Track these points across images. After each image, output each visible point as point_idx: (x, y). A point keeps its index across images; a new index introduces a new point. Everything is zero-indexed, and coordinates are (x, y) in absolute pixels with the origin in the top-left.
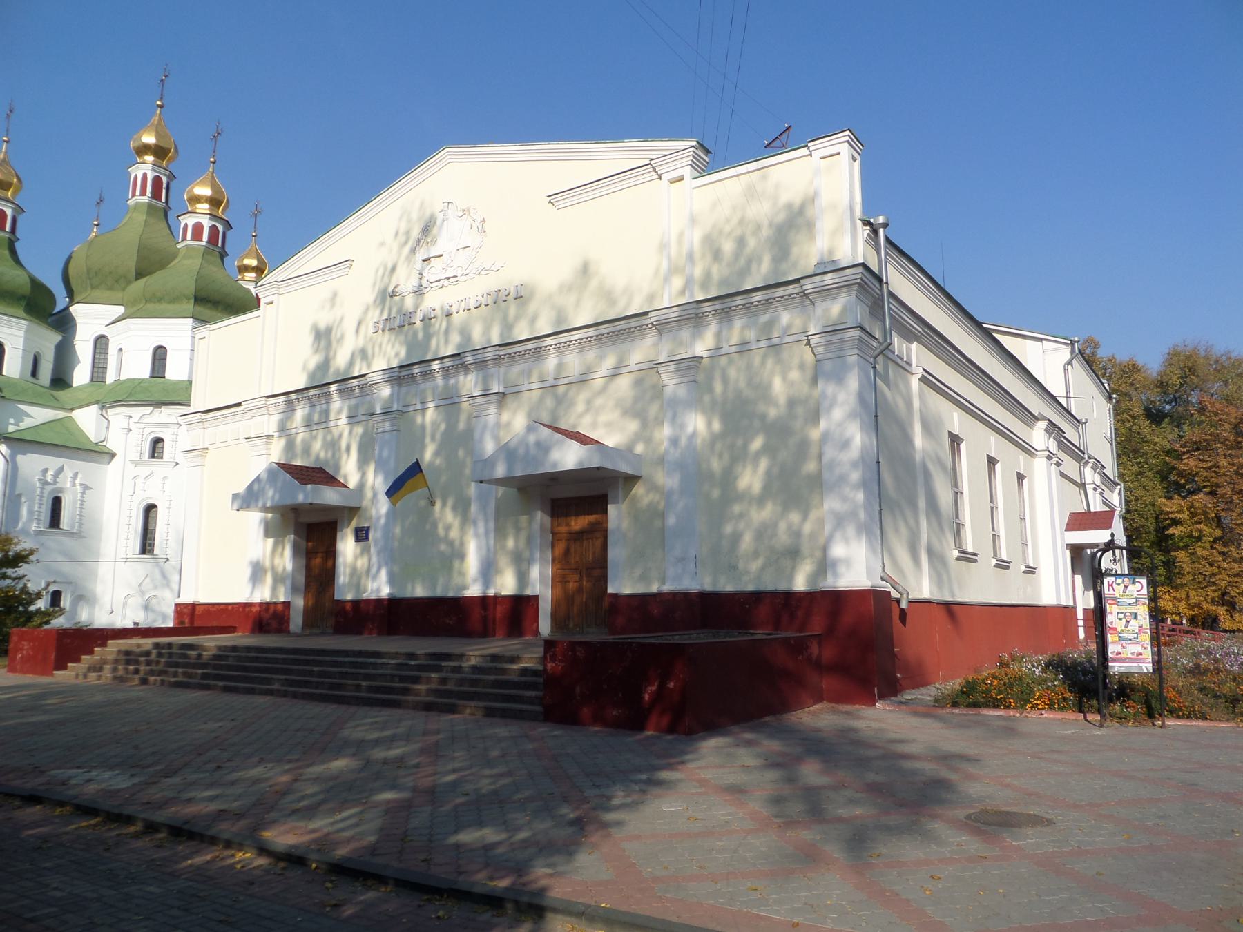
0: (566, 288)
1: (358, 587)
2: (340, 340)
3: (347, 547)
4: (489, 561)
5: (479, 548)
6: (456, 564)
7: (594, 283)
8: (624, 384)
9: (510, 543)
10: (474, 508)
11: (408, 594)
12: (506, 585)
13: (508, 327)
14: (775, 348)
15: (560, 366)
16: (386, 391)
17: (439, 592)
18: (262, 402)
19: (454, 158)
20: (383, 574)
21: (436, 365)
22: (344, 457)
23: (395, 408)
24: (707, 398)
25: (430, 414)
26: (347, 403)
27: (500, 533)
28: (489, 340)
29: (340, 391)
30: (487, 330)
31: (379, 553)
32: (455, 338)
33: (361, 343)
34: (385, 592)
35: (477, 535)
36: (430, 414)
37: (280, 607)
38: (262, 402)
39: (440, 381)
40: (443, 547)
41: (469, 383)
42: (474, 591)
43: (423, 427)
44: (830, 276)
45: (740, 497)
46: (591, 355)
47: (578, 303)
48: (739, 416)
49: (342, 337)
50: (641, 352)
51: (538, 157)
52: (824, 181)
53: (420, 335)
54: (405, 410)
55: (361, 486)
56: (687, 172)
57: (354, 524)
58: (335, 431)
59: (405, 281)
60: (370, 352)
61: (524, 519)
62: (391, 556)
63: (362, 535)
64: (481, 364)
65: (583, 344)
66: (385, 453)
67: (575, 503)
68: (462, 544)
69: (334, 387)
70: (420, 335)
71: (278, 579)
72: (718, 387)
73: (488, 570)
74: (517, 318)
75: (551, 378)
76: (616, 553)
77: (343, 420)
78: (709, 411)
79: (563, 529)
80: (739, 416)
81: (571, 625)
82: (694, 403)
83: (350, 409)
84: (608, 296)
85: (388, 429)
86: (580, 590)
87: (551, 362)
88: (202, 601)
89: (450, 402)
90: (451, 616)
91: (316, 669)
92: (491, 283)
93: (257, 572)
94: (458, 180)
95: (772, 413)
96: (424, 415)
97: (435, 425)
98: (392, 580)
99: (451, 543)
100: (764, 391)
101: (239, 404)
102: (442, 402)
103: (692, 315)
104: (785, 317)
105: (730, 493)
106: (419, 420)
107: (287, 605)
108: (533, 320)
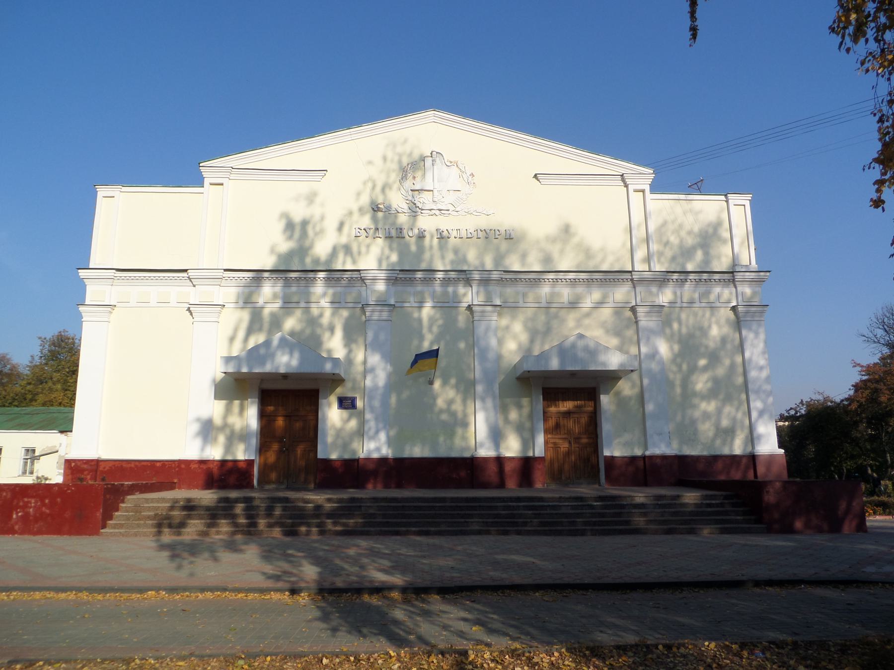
0: (553, 240)
1: (345, 446)
2: (321, 233)
3: (333, 415)
4: (488, 432)
5: (487, 420)
6: (459, 431)
7: (575, 240)
8: (606, 313)
9: (513, 415)
10: (479, 388)
11: (407, 454)
12: (512, 448)
13: (499, 258)
14: (713, 308)
15: (553, 294)
16: (381, 286)
17: (442, 453)
18: (221, 273)
19: (439, 120)
20: (383, 436)
21: (440, 275)
22: (327, 335)
23: (392, 302)
24: (668, 331)
25: (427, 311)
26: (331, 291)
27: (503, 409)
28: (483, 265)
29: (327, 279)
30: (481, 256)
31: (377, 419)
32: (450, 256)
33: (344, 240)
34: (386, 451)
35: (485, 409)
36: (427, 311)
37: (242, 465)
38: (221, 273)
39: (438, 288)
40: (444, 417)
41: (470, 296)
42: (486, 452)
43: (420, 320)
44: (748, 274)
45: (695, 394)
46: (580, 290)
47: (562, 252)
48: (689, 346)
49: (322, 231)
50: (621, 293)
51: (507, 139)
52: (730, 217)
53: (413, 248)
54: (398, 305)
55: (349, 361)
56: (647, 188)
57: (339, 391)
58: (315, 311)
59: (398, 200)
60: (355, 248)
61: (525, 401)
62: (386, 420)
63: (346, 403)
64: (485, 282)
65: (574, 283)
66: (382, 337)
67: (568, 392)
68: (465, 415)
69: (321, 275)
70: (413, 248)
71: (233, 438)
72: (675, 326)
73: (496, 436)
74: (508, 252)
75: (544, 301)
76: (606, 427)
77: (325, 303)
78: (670, 339)
79: (553, 409)
80: (689, 346)
81: (563, 478)
82: (661, 332)
83: (334, 295)
84: (588, 253)
85: (384, 318)
86: (568, 454)
87: (545, 290)
88: (105, 457)
89: (447, 305)
90: (468, 469)
91: (432, 529)
92: (483, 223)
93: (207, 430)
94: (429, 131)
95: (712, 345)
96: (420, 311)
97: (432, 320)
98: (390, 442)
99: (453, 414)
100: (704, 331)
101: (185, 271)
102: (439, 305)
103: (662, 279)
104: (717, 290)
105: (688, 395)
106: (416, 315)
107: (250, 463)
108: (524, 256)
